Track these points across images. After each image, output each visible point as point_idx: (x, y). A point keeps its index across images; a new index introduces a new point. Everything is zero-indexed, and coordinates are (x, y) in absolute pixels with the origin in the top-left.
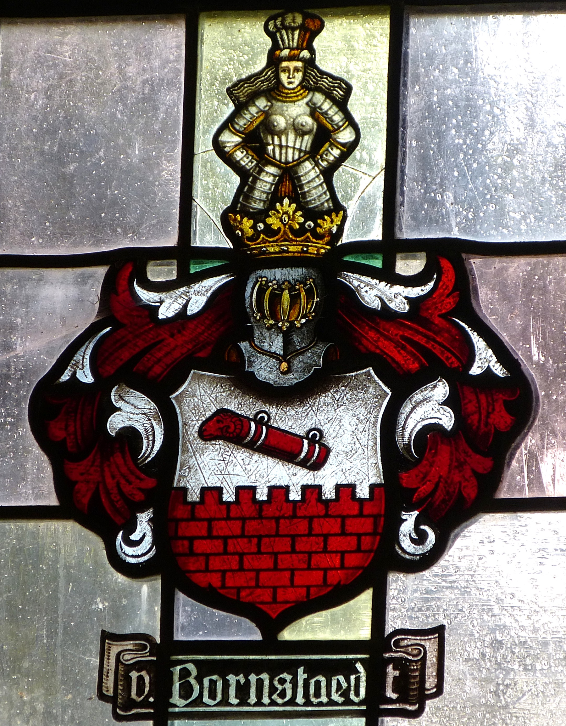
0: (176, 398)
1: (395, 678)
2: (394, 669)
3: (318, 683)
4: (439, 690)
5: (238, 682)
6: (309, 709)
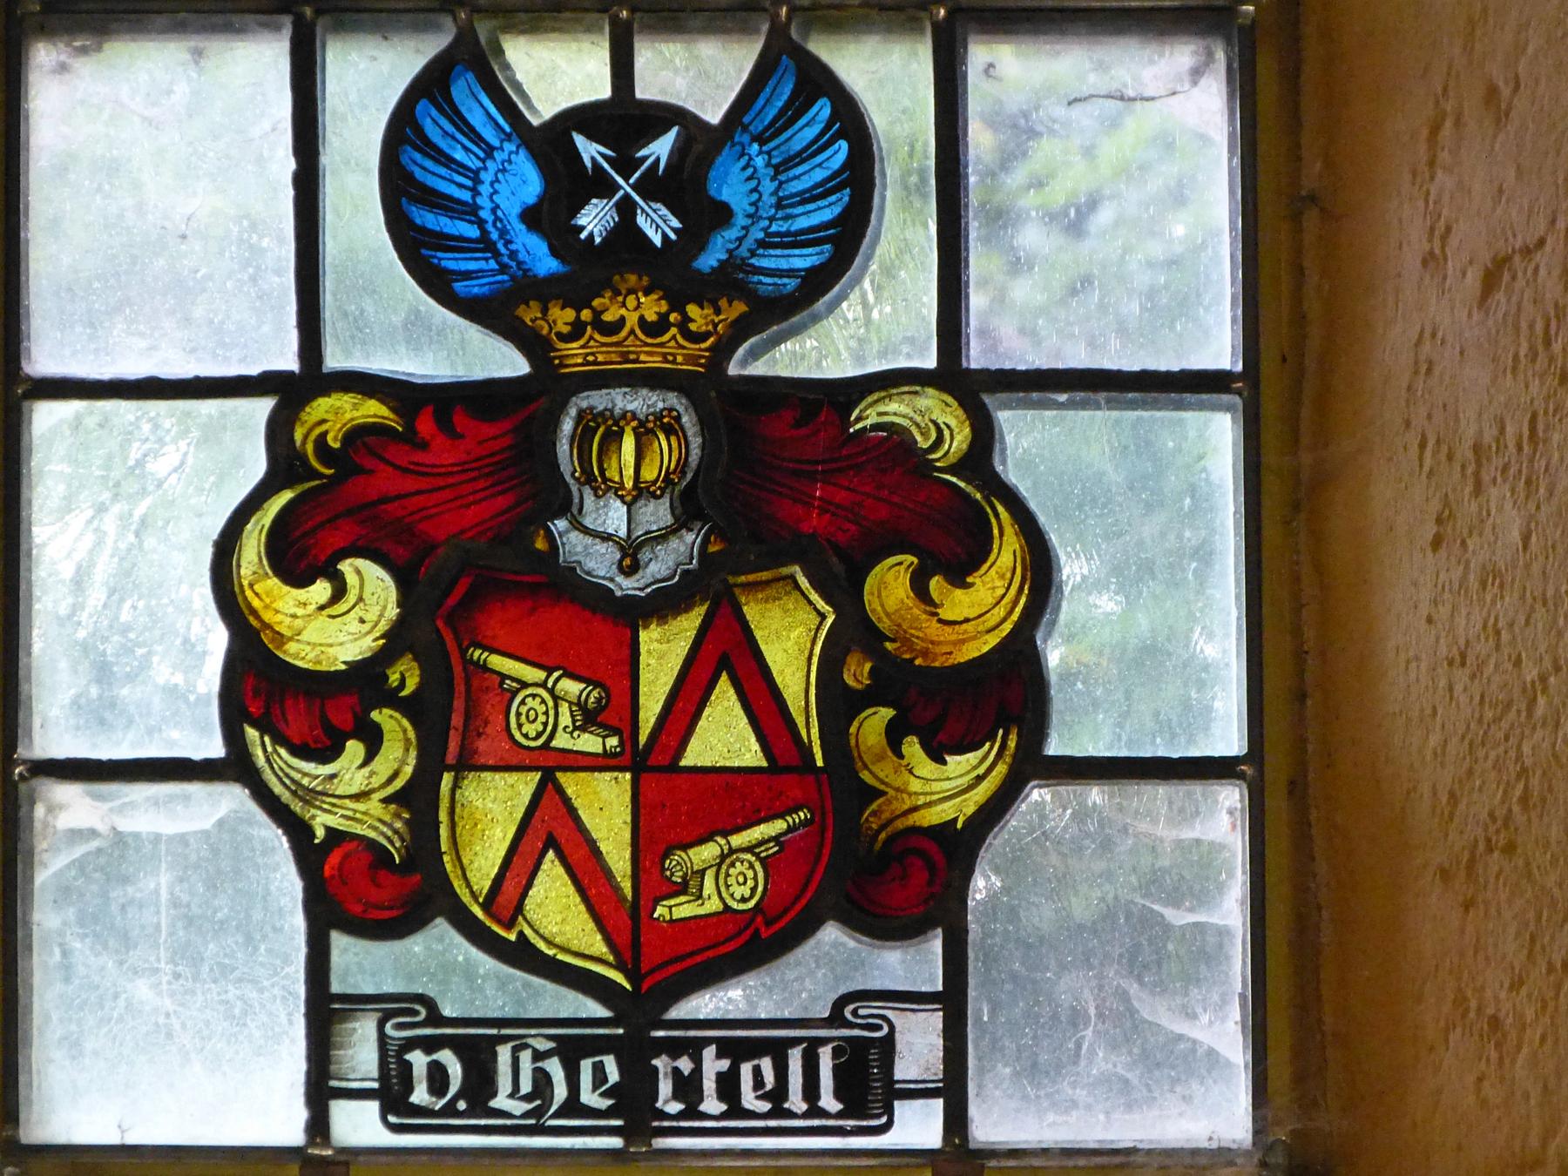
0: (792, 578)
6: (816, 1122)
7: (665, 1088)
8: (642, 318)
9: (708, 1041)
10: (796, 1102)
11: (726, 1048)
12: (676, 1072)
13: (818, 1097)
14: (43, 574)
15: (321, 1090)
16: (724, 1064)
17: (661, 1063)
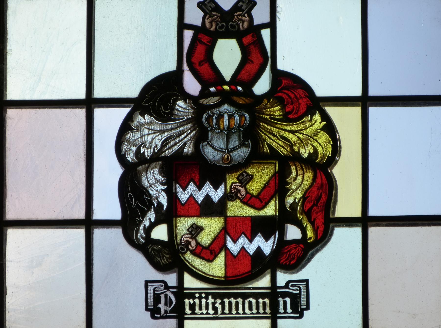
0: (276, 164)
1: (160, 303)
2: (212, 298)
3: (250, 303)
4: (308, 308)
5: (190, 302)
6: (238, 316)
7: (187, 308)
8: (268, 103)
12: (190, 302)
13: (195, 310)
14: (221, 224)
16: (213, 301)
17: (187, 301)
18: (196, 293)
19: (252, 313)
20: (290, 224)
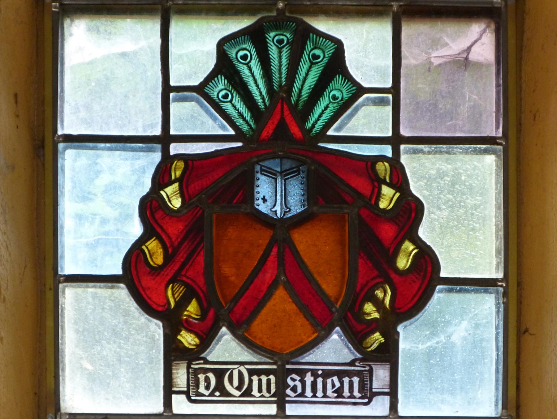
2: (312, 375)
6: (340, 400)
9: (308, 370)
10: (346, 393)
11: (314, 374)
15: (169, 390)
18: (319, 370)
19: (262, 396)
20: (402, 245)
